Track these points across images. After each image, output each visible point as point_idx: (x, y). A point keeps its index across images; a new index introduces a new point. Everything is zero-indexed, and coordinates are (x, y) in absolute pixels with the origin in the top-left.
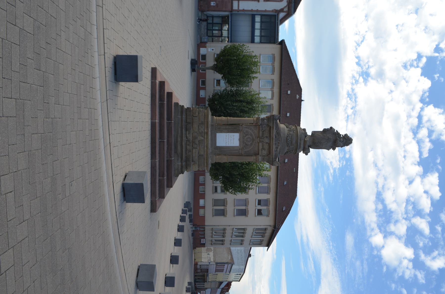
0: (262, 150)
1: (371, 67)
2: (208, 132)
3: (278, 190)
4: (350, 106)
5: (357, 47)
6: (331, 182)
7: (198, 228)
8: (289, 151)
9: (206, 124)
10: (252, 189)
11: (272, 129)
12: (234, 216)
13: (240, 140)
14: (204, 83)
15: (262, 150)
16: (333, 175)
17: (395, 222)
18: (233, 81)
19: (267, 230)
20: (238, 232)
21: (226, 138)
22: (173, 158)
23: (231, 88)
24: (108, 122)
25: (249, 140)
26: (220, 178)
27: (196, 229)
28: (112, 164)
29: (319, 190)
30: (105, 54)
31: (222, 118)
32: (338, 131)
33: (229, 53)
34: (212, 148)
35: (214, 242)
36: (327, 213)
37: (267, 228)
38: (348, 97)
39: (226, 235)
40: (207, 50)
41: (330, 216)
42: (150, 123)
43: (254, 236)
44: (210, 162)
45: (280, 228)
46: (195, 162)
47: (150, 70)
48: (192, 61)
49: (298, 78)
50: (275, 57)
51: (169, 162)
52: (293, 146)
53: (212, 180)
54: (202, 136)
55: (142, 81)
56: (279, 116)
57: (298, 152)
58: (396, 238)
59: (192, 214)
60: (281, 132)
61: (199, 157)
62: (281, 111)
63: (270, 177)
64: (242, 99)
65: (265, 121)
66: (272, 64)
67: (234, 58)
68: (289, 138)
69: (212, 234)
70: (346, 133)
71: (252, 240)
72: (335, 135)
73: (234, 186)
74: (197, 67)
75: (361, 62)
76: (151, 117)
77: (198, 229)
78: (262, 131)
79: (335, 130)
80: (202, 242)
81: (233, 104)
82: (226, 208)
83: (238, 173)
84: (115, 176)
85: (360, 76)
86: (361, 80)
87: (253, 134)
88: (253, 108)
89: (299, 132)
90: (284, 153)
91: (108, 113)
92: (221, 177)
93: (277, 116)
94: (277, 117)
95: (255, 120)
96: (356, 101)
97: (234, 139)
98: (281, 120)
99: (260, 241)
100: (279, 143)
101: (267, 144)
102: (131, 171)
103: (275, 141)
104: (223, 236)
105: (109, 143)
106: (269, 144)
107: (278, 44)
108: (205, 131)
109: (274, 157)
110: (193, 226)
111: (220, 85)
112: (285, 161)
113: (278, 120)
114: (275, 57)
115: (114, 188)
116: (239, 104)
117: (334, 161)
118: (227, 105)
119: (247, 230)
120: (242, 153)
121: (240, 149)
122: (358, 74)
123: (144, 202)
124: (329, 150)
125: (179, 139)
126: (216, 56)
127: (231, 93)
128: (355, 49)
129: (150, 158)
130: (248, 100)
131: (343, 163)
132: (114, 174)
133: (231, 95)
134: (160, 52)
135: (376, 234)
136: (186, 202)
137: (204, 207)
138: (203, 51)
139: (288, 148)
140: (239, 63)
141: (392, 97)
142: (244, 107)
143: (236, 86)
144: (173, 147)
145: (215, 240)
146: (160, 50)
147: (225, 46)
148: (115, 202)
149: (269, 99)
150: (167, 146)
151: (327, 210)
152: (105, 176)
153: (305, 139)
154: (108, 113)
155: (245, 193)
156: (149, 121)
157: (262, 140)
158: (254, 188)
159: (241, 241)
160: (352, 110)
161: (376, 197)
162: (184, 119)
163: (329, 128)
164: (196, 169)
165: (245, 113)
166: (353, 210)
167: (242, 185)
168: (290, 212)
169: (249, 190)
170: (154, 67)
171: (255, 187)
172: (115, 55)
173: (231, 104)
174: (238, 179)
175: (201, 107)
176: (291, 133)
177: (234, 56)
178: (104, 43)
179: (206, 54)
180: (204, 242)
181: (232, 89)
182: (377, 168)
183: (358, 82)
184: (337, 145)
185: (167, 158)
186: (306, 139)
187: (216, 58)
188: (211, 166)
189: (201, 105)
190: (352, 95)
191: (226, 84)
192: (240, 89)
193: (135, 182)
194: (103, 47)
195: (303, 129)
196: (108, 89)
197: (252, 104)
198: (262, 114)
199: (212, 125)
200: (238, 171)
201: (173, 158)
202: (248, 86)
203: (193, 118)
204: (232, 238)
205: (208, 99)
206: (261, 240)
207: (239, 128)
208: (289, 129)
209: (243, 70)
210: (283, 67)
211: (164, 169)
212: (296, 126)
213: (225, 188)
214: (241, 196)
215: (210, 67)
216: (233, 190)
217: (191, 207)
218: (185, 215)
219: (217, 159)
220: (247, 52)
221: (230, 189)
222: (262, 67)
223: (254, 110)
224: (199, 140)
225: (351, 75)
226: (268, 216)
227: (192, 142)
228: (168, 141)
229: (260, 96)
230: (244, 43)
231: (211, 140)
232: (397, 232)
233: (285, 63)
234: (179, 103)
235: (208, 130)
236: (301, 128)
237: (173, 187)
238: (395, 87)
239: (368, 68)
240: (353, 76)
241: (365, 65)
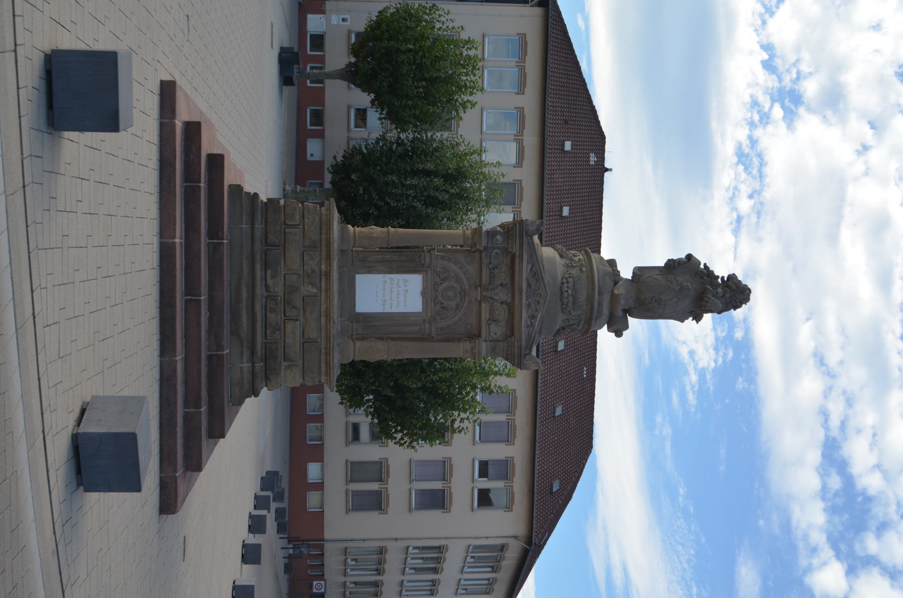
0: (489, 324)
1: (805, 77)
2: (330, 270)
3: (538, 433)
4: (745, 189)
5: (767, 16)
6: (693, 410)
7: (303, 549)
8: (568, 326)
9: (324, 249)
10: (463, 433)
11: (517, 261)
12: (410, 510)
13: (424, 293)
14: (318, 118)
15: (489, 322)
16: (696, 389)
17: (878, 529)
18: (406, 114)
19: (507, 549)
20: (423, 558)
21: (384, 290)
22: (227, 351)
23: (399, 133)
24: (29, 253)
25: (450, 294)
26: (368, 401)
27: (297, 551)
28: (39, 379)
29: (657, 432)
30: (18, 47)
31: (372, 231)
32: (708, 268)
33: (391, 32)
34: (342, 319)
35: (351, 588)
36: (681, 499)
37: (507, 544)
38: (739, 162)
39: (386, 566)
40: (328, 21)
41: (692, 509)
42: (156, 247)
43: (469, 567)
44: (337, 359)
45: (545, 543)
46: (291, 360)
47: (156, 89)
48: (283, 55)
49: (595, 103)
50: (526, 43)
51: (216, 363)
52: (579, 312)
53: (342, 407)
54: (313, 285)
55: (132, 126)
56: (538, 222)
57: (593, 329)
58: (881, 575)
59: (285, 507)
60: (543, 269)
61: (305, 345)
62: (545, 201)
63: (515, 392)
64: (430, 166)
65: (499, 237)
66: (516, 138)
67: (408, 45)
68: (567, 287)
69: (345, 566)
70: (731, 273)
71: (462, 581)
72: (701, 278)
73: (409, 424)
74: (299, 73)
75: (778, 62)
76: (158, 227)
77: (304, 550)
78: (489, 268)
79: (700, 263)
80: (315, 591)
81: (406, 180)
82: (386, 486)
83: (419, 385)
84: (51, 412)
85: (773, 101)
86: (778, 112)
87: (463, 276)
88: (463, 193)
89: (597, 270)
90: (555, 332)
91: (27, 227)
92: (371, 397)
93: (533, 222)
94: (532, 228)
95: (470, 236)
96: (761, 176)
97: (407, 291)
98: (544, 235)
99: (486, 582)
100: (539, 303)
101: (504, 306)
102: (100, 397)
103: (527, 297)
104: (377, 570)
105: (32, 317)
106: (511, 308)
107: (535, 4)
108: (322, 270)
109: (524, 343)
110: (288, 544)
111: (365, 123)
112: (556, 347)
113: (535, 234)
114: (527, 74)
115: (47, 450)
116: (423, 182)
117: (700, 349)
118: (387, 184)
119: (447, 551)
120: (431, 333)
121: (424, 321)
122: (768, 97)
123: (139, 490)
124: (682, 321)
125: (244, 294)
126: (353, 40)
127: (400, 149)
128: (760, 22)
129: (157, 353)
130: (449, 168)
131: (725, 356)
132: (48, 410)
133: (398, 154)
134: (186, 32)
135: (825, 564)
136: (267, 473)
137: (319, 486)
138: (315, 23)
139: (565, 317)
140: (421, 59)
141: (866, 163)
142: (437, 189)
143: (414, 129)
144: (227, 317)
145: (355, 583)
146: (186, 27)
147: (380, 9)
148: (50, 493)
149: (511, 165)
150: (208, 314)
151: (681, 491)
152: (19, 416)
153: (612, 291)
154: (29, 224)
155: (440, 444)
156: (155, 241)
157: (489, 294)
158: (467, 428)
159: (430, 583)
160: (752, 202)
161: (824, 455)
162: (258, 234)
163: (683, 256)
164: (297, 382)
165: (440, 209)
166: (756, 492)
167: (433, 419)
168: (575, 495)
169: (452, 433)
170: (169, 78)
171: (470, 426)
172: (47, 48)
173: (397, 181)
174: (421, 401)
175: (311, 189)
176: (574, 272)
177: (406, 41)
178: (14, 16)
179: (325, 32)
180: (323, 590)
181: (403, 136)
182: (824, 368)
183: (768, 118)
184: (706, 306)
185: (209, 349)
186: (616, 292)
187: (353, 44)
188: (339, 373)
189: (311, 183)
190: (750, 157)
191: (383, 120)
192: (425, 138)
193: (114, 430)
194: (12, 27)
195: (607, 261)
196: (29, 154)
197: (460, 182)
198: (490, 210)
199: (342, 252)
200: (421, 379)
201: (227, 351)
202: (448, 128)
203: (287, 230)
204: (404, 575)
205: (332, 166)
206: (488, 580)
207: (423, 260)
208: (568, 262)
209: (433, 81)
210: (549, 73)
211: (200, 383)
212: (587, 253)
213: (381, 428)
214: (428, 451)
215: (336, 71)
216: (406, 435)
217: (282, 487)
218: (264, 512)
219: (357, 351)
220: (444, 27)
221: (396, 432)
222: (489, 72)
223: (465, 200)
224: (303, 296)
225: (748, 99)
226: (509, 508)
227: (283, 300)
228: (211, 299)
229: (484, 159)
230: (435, 2)
231: (341, 293)
232: (884, 558)
233: (555, 59)
234: (242, 185)
235: (330, 267)
236: (602, 259)
237: (228, 436)
238: (875, 134)
239: (798, 78)
240: (753, 101)
241: (788, 71)
